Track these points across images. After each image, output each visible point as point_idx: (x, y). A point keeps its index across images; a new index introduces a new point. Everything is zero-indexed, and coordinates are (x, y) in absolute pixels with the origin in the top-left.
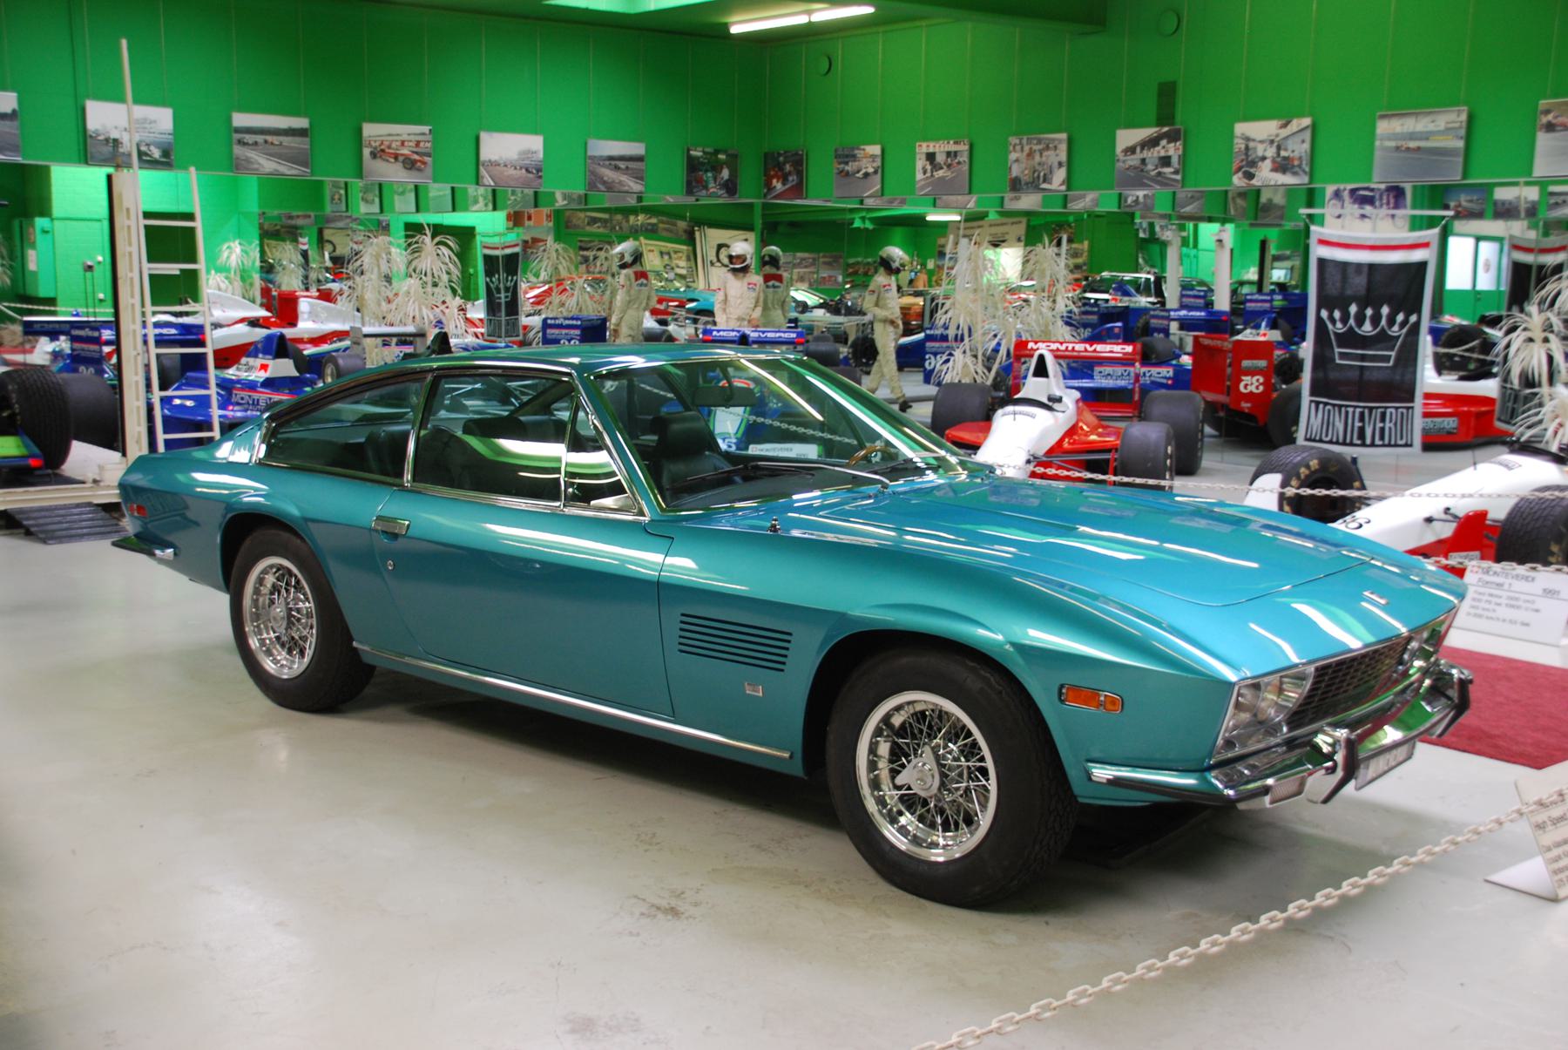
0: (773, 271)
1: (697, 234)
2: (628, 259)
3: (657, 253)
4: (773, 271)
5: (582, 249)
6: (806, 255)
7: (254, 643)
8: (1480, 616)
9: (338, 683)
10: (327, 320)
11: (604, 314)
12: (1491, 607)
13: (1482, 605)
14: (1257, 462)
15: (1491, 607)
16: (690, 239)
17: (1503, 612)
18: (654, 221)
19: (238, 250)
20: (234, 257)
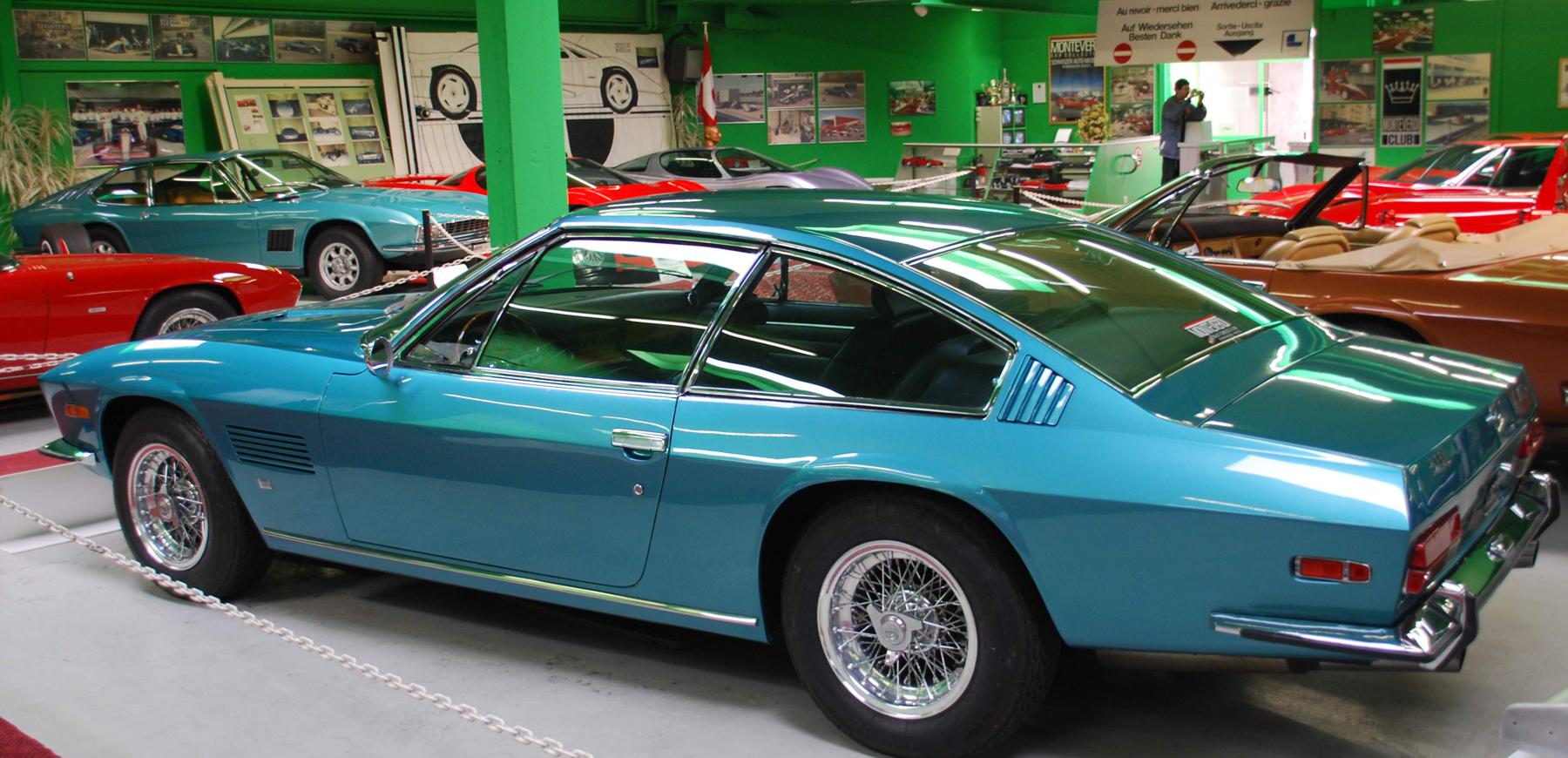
1: (383, 49)
3: (263, 107)
5: (74, 105)
6: (790, 77)
7: (140, 530)
9: (247, 570)
16: (363, 59)
18: (261, 30)
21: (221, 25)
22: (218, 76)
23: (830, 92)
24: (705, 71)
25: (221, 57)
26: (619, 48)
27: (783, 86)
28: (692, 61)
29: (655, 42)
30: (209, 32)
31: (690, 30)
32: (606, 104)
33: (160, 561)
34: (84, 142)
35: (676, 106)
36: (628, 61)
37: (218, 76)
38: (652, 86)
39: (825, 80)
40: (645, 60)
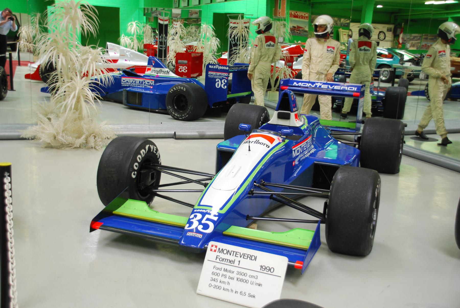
0: (366, 39)
2: (262, 28)
4: (366, 39)
6: (417, 35)
8: (219, 288)
10: (131, 59)
11: (121, 43)
12: (226, 280)
13: (220, 278)
14: (317, 156)
15: (226, 280)
17: (235, 285)
19: (135, 25)
20: (133, 29)
21: (342, 20)
22: (341, 29)
23: (430, 39)
24: (401, 33)
25: (341, 26)
26: (384, 27)
27: (414, 37)
28: (399, 31)
29: (392, 26)
30: (340, 21)
31: (400, 25)
32: (379, 38)
33: (56, 145)
34: (200, 25)
35: (394, 40)
36: (385, 30)
37: (341, 29)
38: (390, 36)
39: (424, 36)
40: (389, 30)
